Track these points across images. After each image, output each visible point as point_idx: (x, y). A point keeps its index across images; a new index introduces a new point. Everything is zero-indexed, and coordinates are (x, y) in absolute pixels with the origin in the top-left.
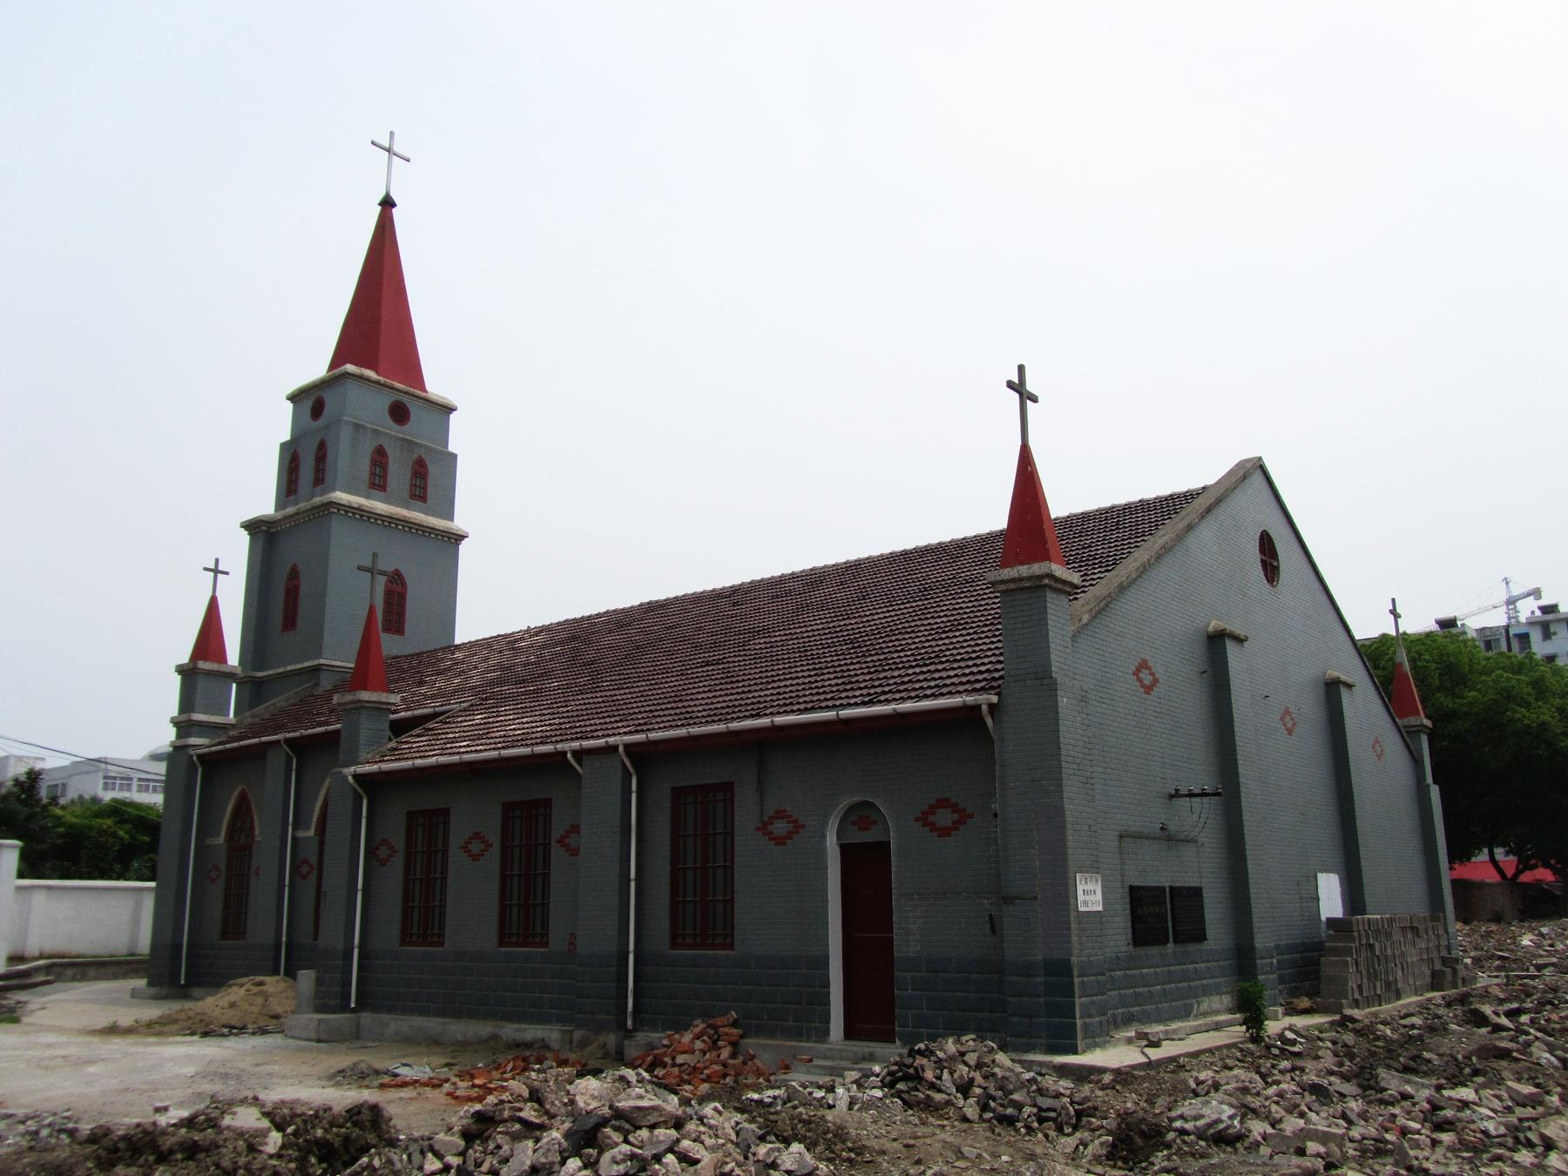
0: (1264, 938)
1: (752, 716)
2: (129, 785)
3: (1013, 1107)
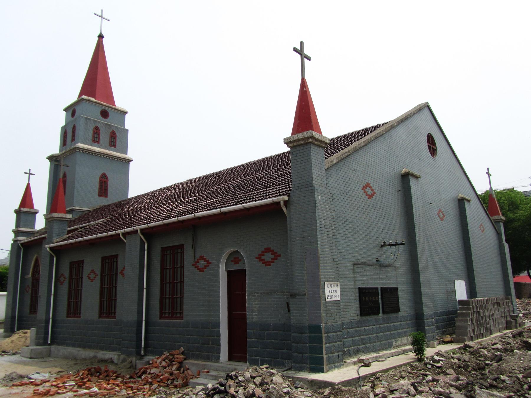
0: (428, 310)
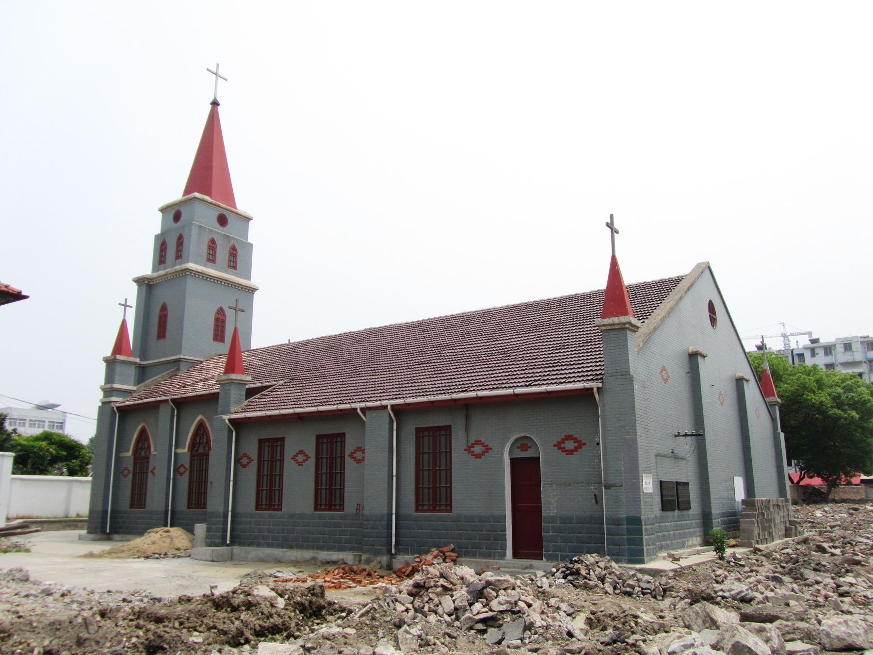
0: (716, 510)
1: (463, 391)
2: (24, 423)
3: (630, 587)
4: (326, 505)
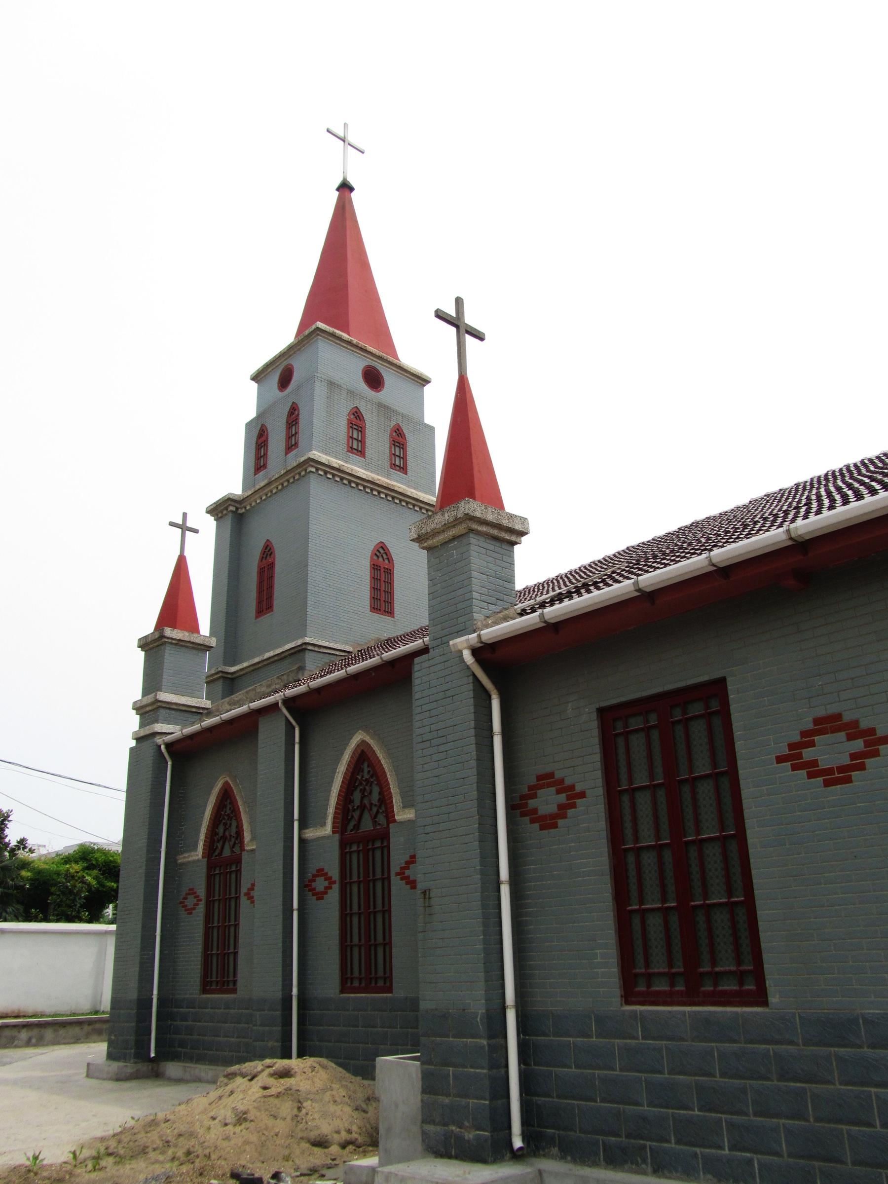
4: (672, 978)
